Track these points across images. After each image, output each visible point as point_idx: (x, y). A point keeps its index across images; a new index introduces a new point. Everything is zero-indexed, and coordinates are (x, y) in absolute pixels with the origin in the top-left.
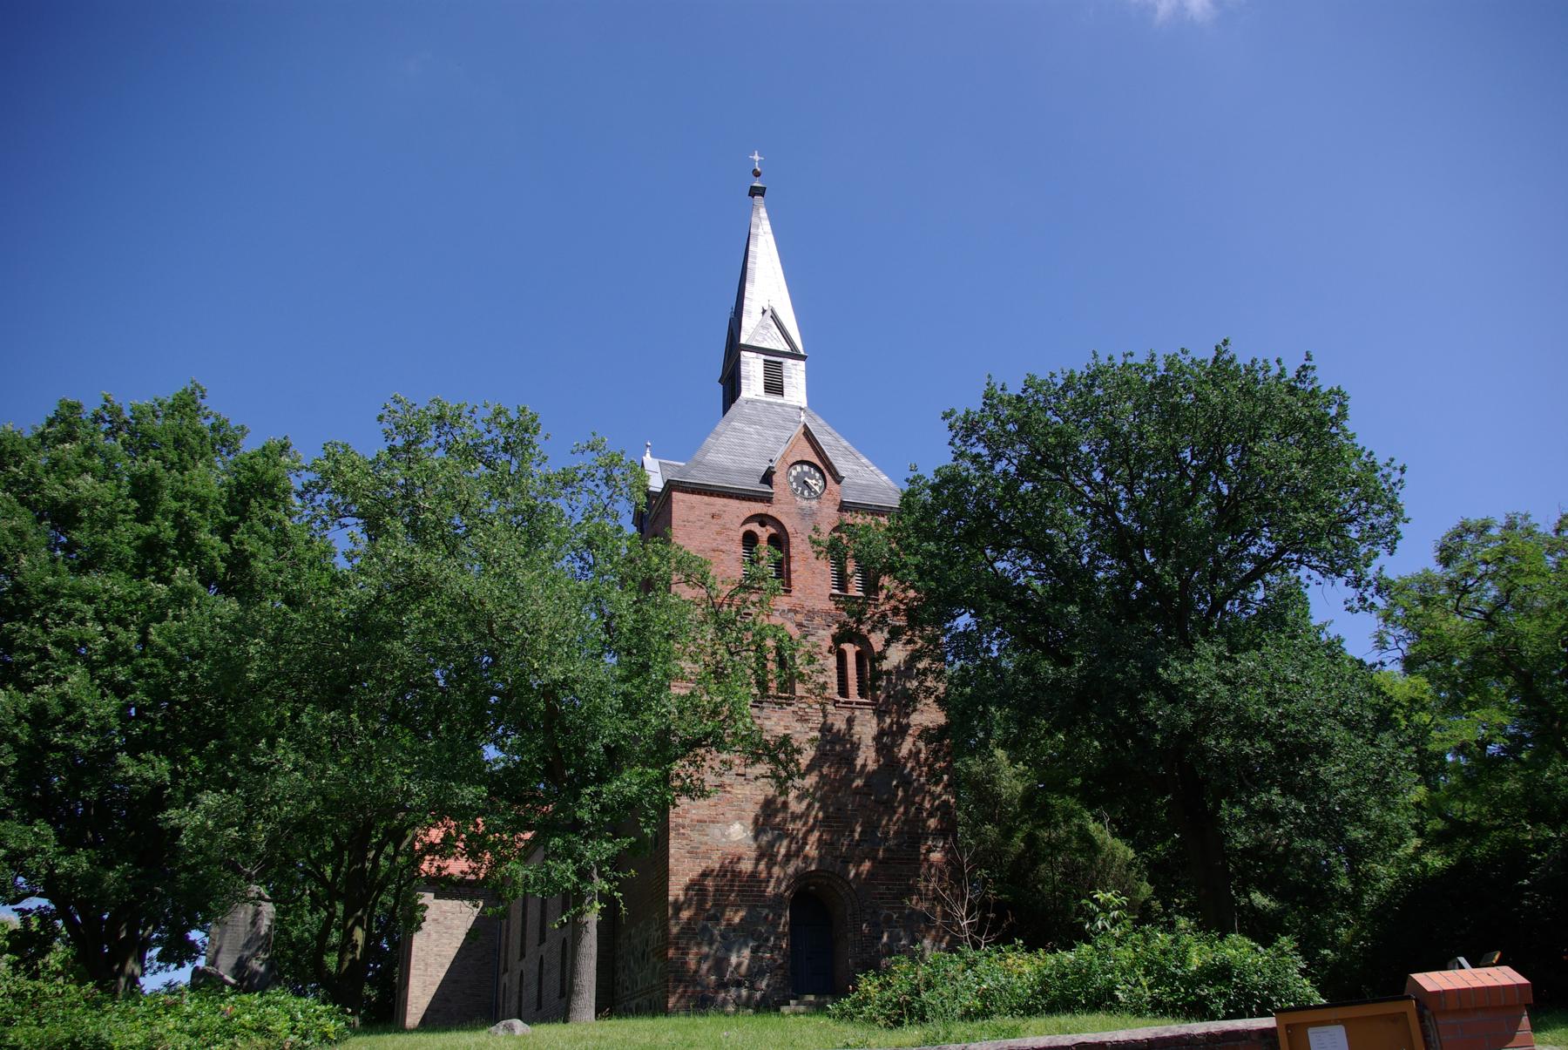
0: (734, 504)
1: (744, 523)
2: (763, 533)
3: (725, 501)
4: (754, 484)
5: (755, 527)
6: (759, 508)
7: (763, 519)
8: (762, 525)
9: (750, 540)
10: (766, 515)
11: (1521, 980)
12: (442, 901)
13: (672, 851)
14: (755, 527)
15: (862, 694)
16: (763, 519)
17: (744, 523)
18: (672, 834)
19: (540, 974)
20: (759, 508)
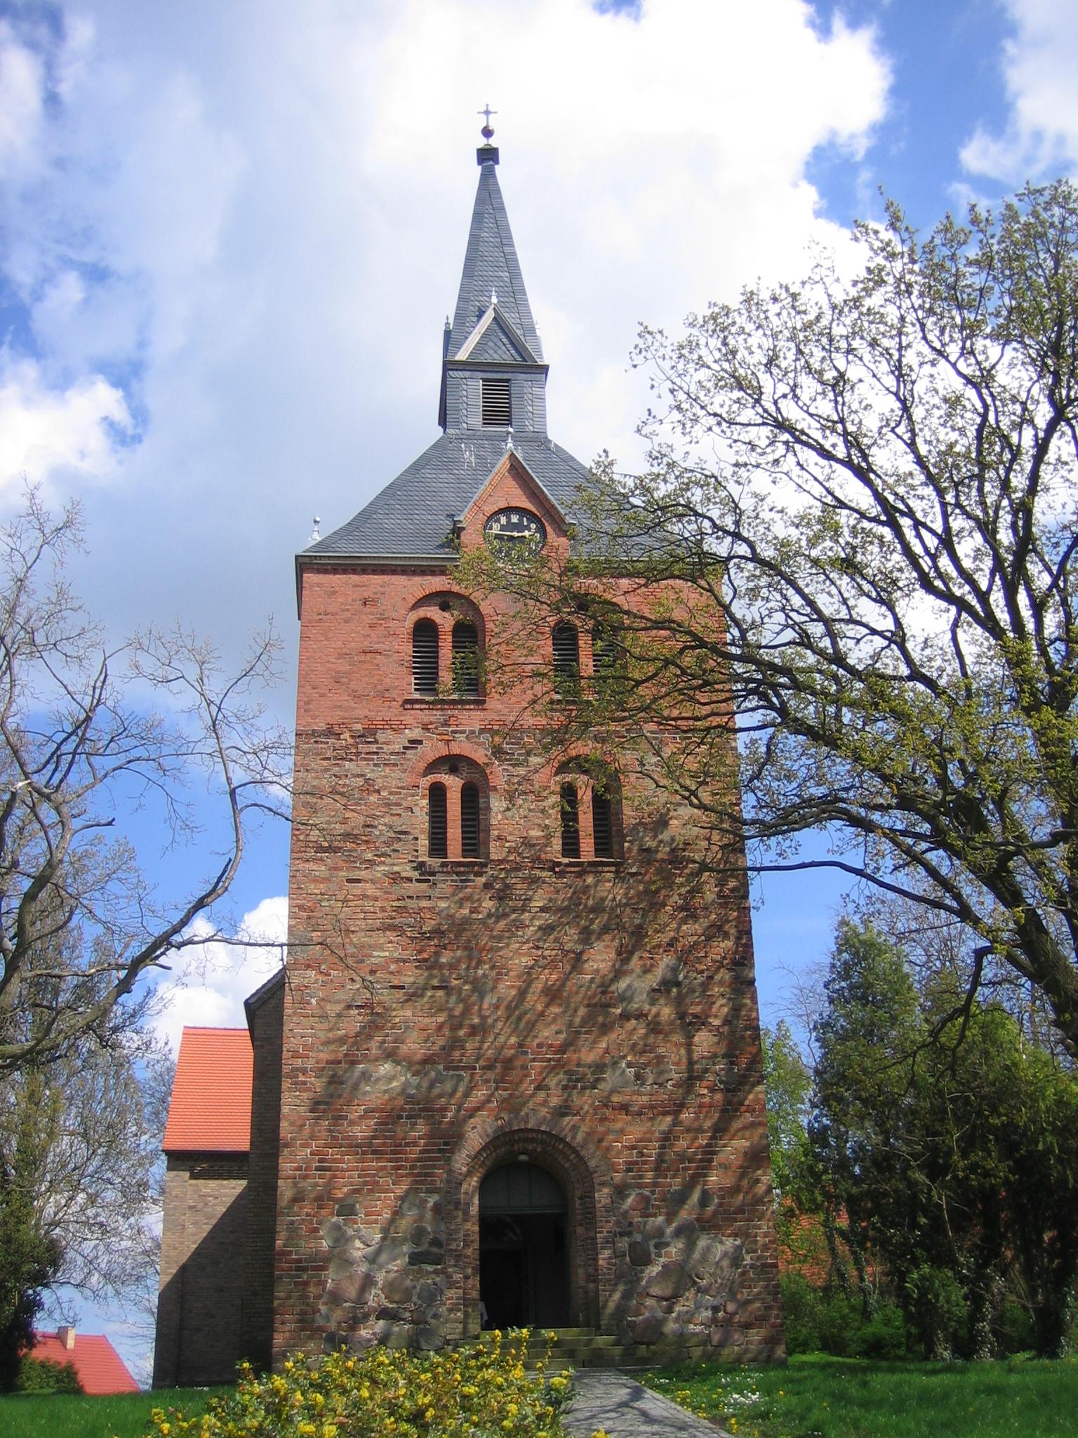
0: (399, 581)
1: (415, 607)
2: (445, 620)
3: (386, 578)
4: (426, 551)
5: (433, 613)
6: (438, 583)
7: (444, 600)
8: (444, 607)
9: (425, 632)
10: (449, 593)
11: (244, 1183)
12: (201, 1182)
13: (285, 1110)
14: (433, 613)
15: (599, 851)
16: (444, 600)
17: (415, 607)
18: (286, 1084)
19: (267, 945)
20: (438, 583)
